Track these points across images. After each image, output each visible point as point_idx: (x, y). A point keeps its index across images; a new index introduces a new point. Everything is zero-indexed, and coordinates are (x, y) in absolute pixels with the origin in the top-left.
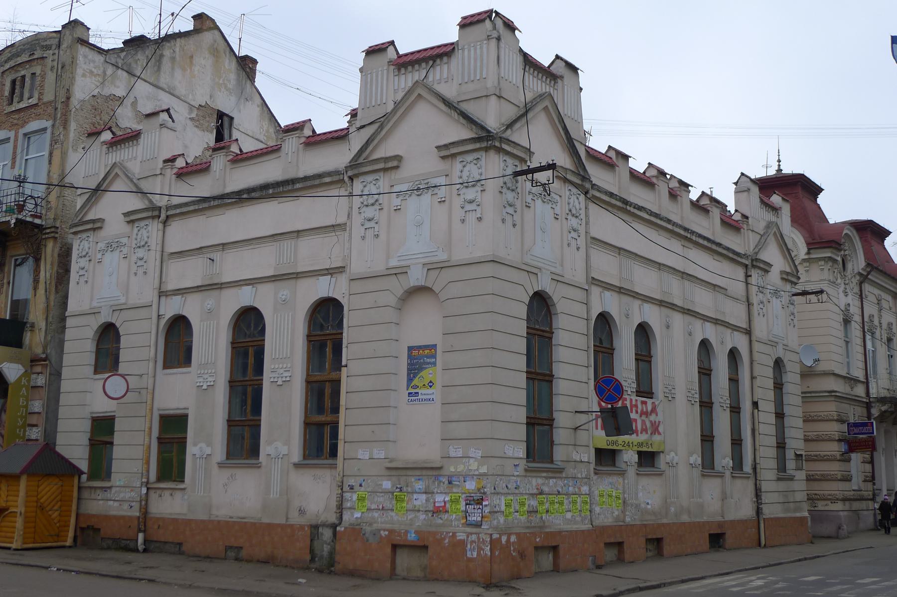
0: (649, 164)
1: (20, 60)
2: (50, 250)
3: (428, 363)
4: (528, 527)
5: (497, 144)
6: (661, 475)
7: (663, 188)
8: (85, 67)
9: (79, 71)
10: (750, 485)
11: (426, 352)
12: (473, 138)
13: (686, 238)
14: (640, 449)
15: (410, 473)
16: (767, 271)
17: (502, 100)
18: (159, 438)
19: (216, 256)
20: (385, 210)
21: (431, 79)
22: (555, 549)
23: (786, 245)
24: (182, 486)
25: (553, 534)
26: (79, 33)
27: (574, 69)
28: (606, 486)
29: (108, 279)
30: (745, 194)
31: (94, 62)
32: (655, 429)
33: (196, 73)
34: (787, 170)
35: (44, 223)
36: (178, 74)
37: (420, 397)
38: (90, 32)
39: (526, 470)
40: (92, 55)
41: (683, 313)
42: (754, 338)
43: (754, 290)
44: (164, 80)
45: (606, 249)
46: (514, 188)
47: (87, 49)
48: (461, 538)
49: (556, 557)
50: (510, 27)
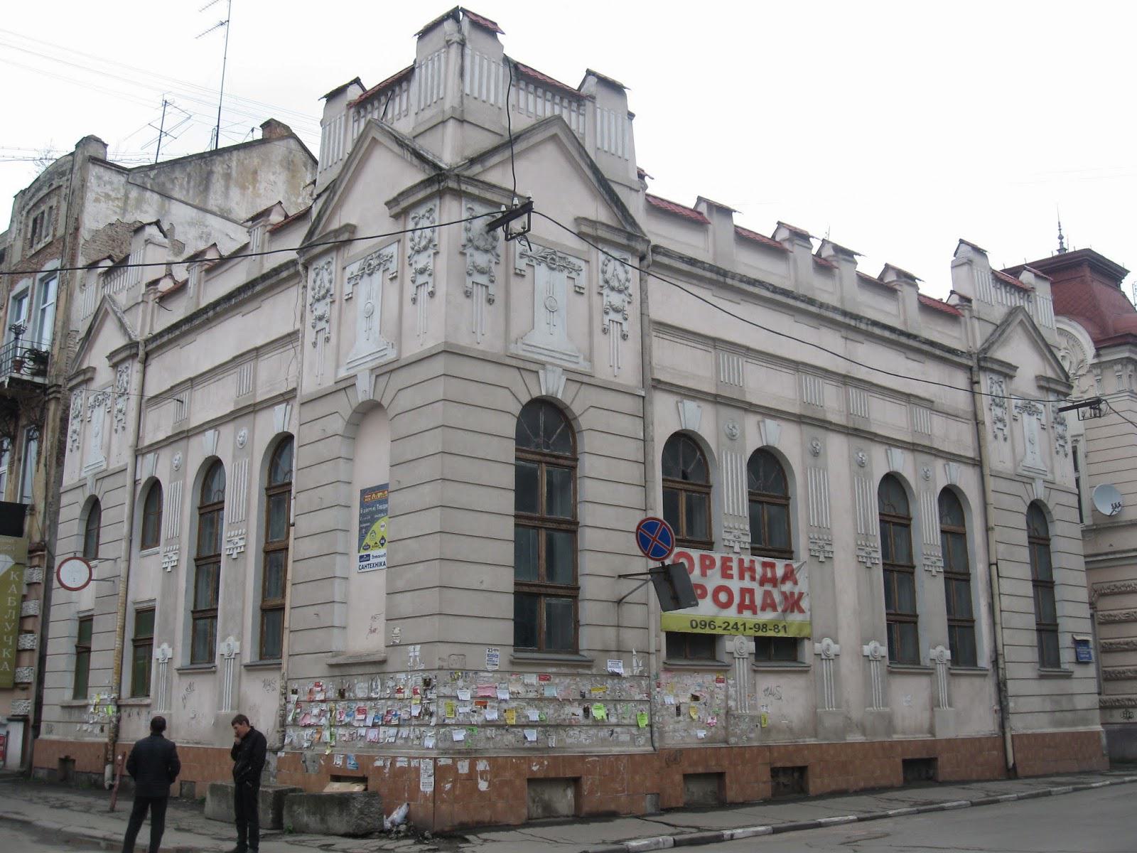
0: (779, 223)
1: (41, 194)
2: (53, 410)
3: (381, 511)
4: (514, 749)
5: (452, 184)
6: (806, 672)
7: (803, 257)
8: (99, 190)
9: (90, 196)
10: (989, 686)
11: (379, 494)
12: (422, 182)
13: (848, 327)
14: (760, 634)
15: (354, 671)
16: (1011, 377)
17: (466, 125)
18: (134, 641)
19: (185, 396)
20: (337, 303)
21: (390, 116)
22: (575, 782)
23: (1043, 339)
24: (147, 701)
25: (569, 761)
26: (93, 150)
27: (616, 88)
28: (679, 689)
29: (97, 443)
30: (965, 268)
31: (111, 183)
32: (793, 603)
33: (262, 191)
34: (1073, 245)
35: (47, 382)
36: (235, 193)
37: (372, 561)
38: (108, 149)
39: (512, 663)
40: (108, 175)
41: (848, 434)
42: (987, 471)
43: (985, 401)
44: (214, 201)
45: (688, 339)
46: (489, 247)
47: (102, 170)
48: (403, 764)
49: (578, 796)
50: (488, 29)
